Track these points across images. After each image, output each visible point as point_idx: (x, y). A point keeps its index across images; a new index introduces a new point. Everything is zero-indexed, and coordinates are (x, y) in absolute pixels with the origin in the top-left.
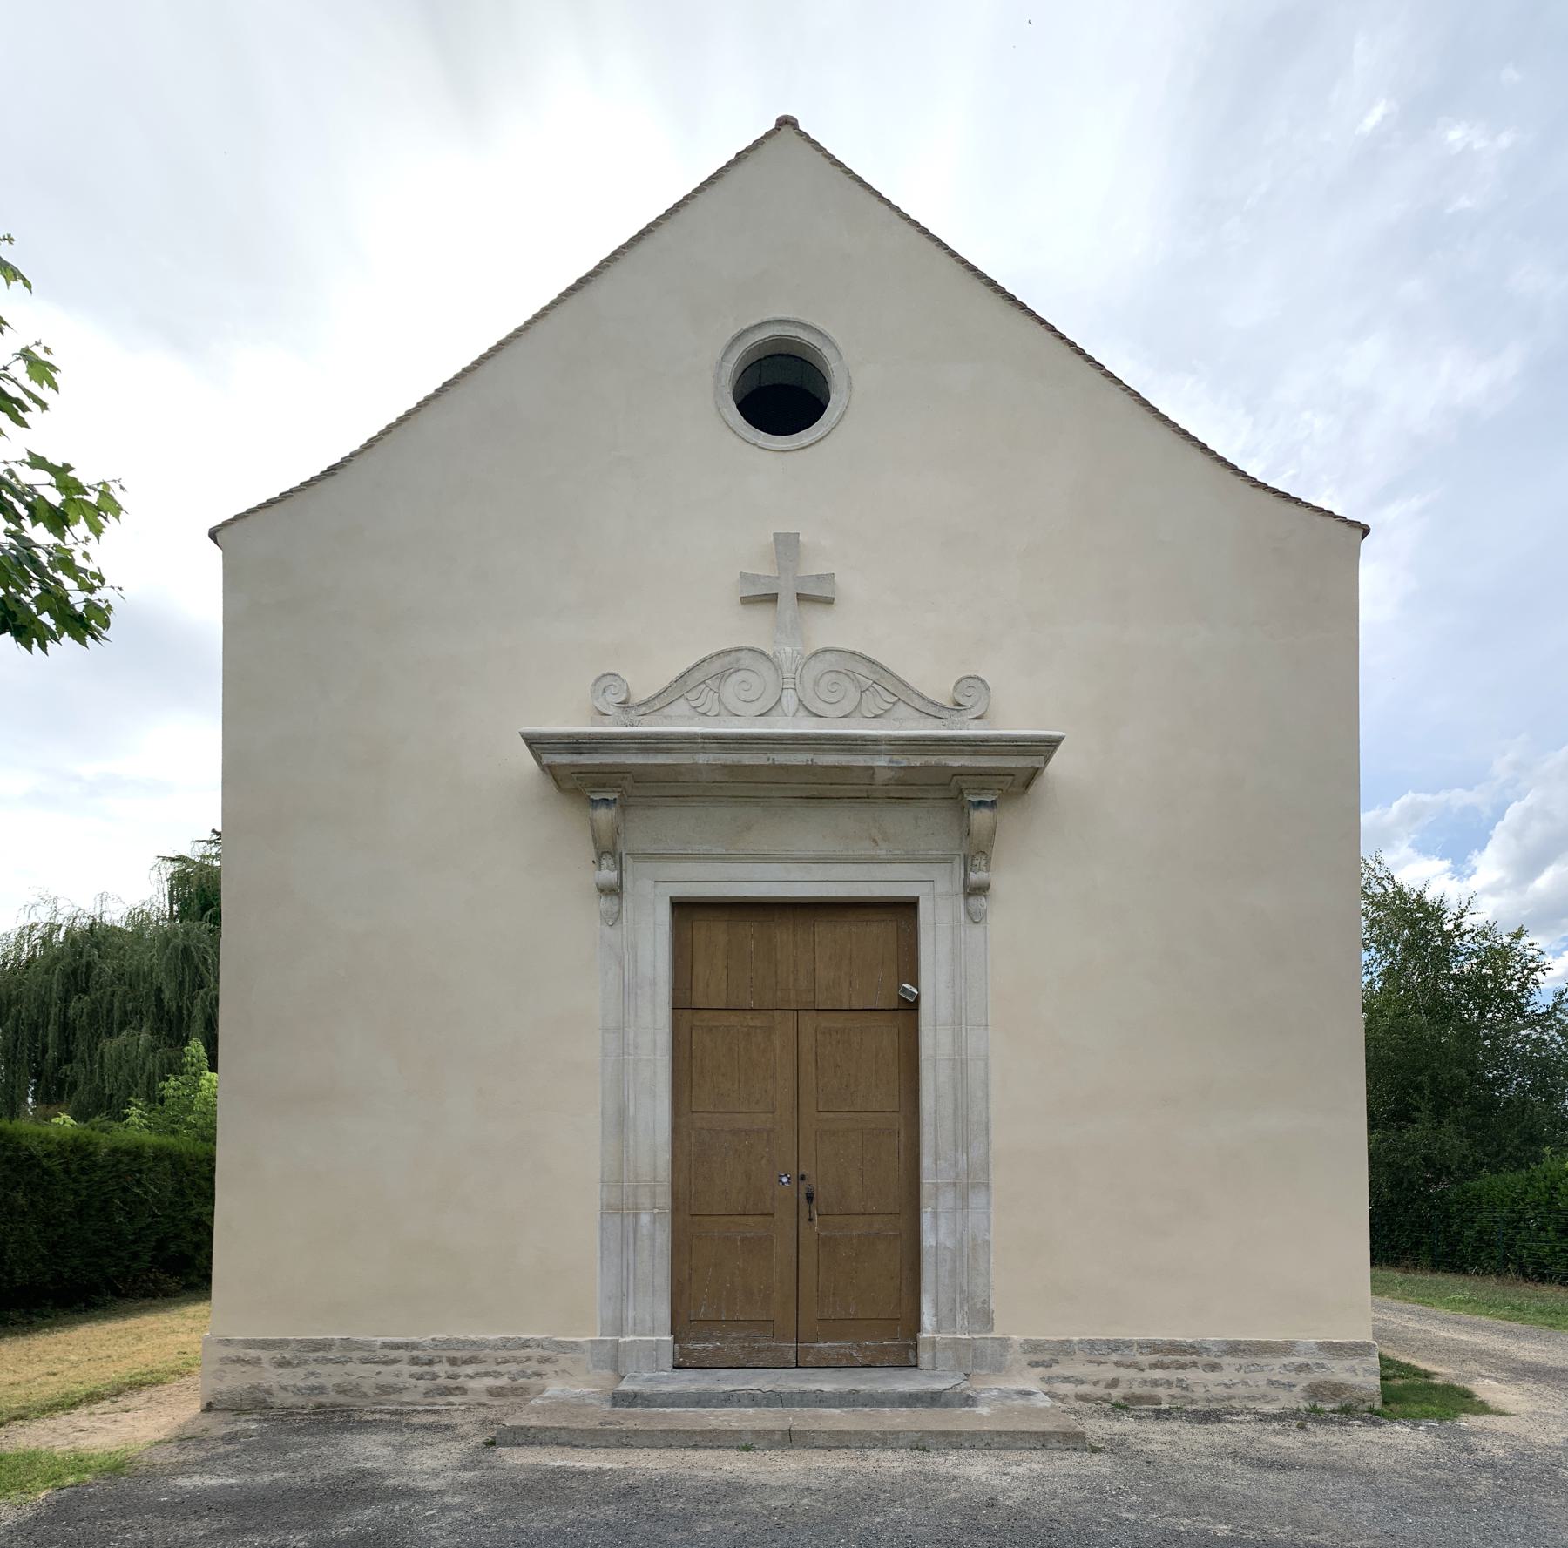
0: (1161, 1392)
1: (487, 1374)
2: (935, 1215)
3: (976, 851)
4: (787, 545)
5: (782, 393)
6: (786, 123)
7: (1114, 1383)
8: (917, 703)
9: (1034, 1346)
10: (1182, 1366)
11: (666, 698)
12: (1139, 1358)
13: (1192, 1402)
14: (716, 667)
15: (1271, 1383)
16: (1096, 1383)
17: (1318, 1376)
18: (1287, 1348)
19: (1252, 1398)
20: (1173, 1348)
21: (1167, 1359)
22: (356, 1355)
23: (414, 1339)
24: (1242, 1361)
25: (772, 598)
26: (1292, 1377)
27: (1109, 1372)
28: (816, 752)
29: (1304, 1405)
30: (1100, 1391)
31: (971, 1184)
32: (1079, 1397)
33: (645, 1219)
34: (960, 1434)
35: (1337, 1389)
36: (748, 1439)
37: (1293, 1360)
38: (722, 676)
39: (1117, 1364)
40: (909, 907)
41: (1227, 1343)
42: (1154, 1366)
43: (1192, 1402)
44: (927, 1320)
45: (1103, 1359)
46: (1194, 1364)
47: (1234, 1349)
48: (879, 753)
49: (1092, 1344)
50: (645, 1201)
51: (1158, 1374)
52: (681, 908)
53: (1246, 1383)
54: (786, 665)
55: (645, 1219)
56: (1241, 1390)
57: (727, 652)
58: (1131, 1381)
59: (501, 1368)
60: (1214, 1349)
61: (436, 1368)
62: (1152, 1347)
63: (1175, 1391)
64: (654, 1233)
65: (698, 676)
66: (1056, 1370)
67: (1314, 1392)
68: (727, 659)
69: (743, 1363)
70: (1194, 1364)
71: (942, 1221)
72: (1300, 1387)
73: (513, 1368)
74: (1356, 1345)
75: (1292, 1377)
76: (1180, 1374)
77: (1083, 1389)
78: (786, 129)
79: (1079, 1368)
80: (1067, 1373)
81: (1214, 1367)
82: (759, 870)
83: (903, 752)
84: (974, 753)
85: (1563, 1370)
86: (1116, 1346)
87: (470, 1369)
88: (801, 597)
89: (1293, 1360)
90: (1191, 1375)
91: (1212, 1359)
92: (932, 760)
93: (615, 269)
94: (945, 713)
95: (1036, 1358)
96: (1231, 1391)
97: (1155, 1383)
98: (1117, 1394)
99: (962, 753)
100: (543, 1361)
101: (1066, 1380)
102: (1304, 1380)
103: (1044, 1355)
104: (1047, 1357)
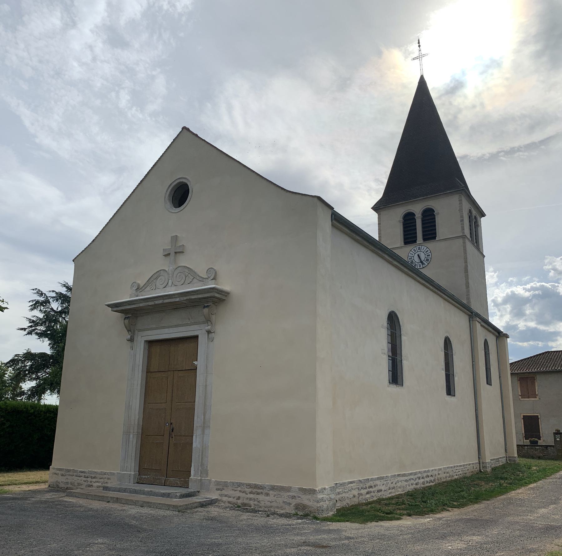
0: (252, 503)
1: (97, 482)
2: (196, 437)
3: (208, 321)
4: (175, 239)
5: (180, 195)
6: (184, 128)
7: (239, 498)
8: (198, 278)
9: (218, 483)
10: (258, 494)
11: (145, 286)
12: (246, 490)
13: (260, 507)
14: (155, 277)
15: (284, 502)
16: (234, 498)
17: (298, 501)
18: (288, 489)
19: (278, 507)
20: (256, 486)
21: (254, 490)
22: (75, 474)
23: (85, 470)
24: (275, 493)
25: (169, 254)
26: (290, 501)
27: (238, 494)
28: (164, 299)
29: (294, 512)
30: (234, 500)
31: (205, 426)
32: (229, 502)
33: (131, 436)
34: (151, 503)
35: (304, 507)
36: (109, 499)
37: (290, 494)
38: (157, 278)
39: (240, 491)
40: (196, 337)
41: (271, 486)
42: (251, 493)
43: (260, 507)
44: (192, 472)
45: (235, 489)
46: (262, 493)
47: (273, 488)
48: (176, 298)
49: (233, 483)
50: (132, 431)
51: (252, 496)
52: (150, 343)
53: (276, 502)
54: (170, 273)
55: (131, 436)
56: (274, 504)
57: (158, 272)
58: (244, 498)
59: (100, 480)
60: (267, 488)
61: (88, 479)
62: (249, 486)
63: (256, 503)
64: (134, 441)
65: (152, 279)
66: (224, 492)
67: (297, 507)
68: (158, 273)
69: (144, 482)
70: (262, 493)
71: (198, 439)
72: (293, 505)
73: (102, 480)
74: (310, 489)
75: (290, 501)
76: (258, 496)
77: (230, 499)
78: (184, 130)
79: (230, 493)
80: (226, 493)
81: (267, 495)
82: (166, 330)
83: (182, 296)
84: (198, 294)
85: (559, 527)
86: (239, 485)
87: (94, 480)
88: (176, 253)
89: (290, 494)
90: (261, 497)
91: (267, 491)
92: (188, 298)
93: (148, 176)
94: (204, 280)
95: (218, 487)
96: (272, 504)
97: (251, 499)
98: (239, 502)
99: (194, 295)
100: (108, 479)
101: (226, 496)
102: (294, 502)
103: (221, 486)
104: (221, 487)
